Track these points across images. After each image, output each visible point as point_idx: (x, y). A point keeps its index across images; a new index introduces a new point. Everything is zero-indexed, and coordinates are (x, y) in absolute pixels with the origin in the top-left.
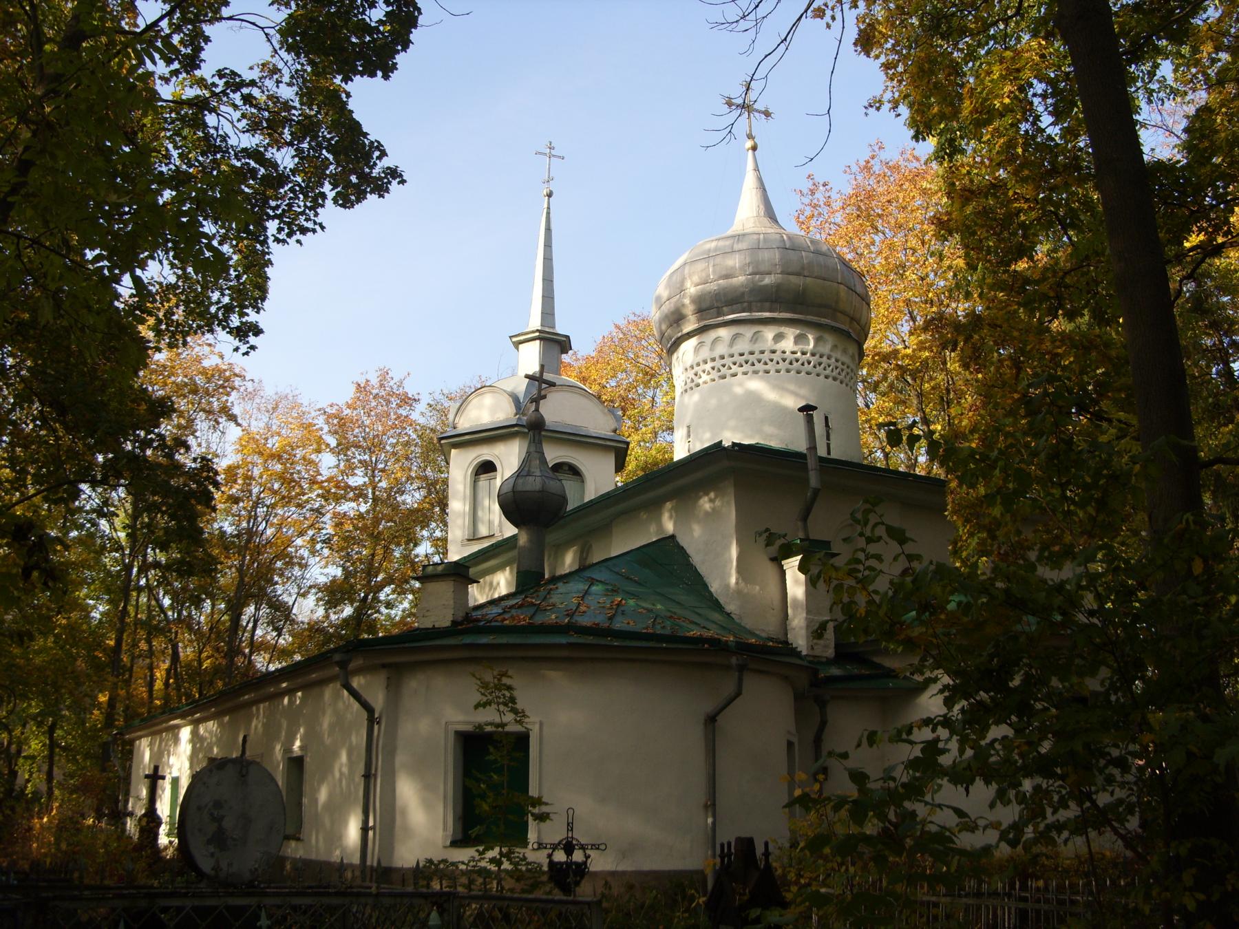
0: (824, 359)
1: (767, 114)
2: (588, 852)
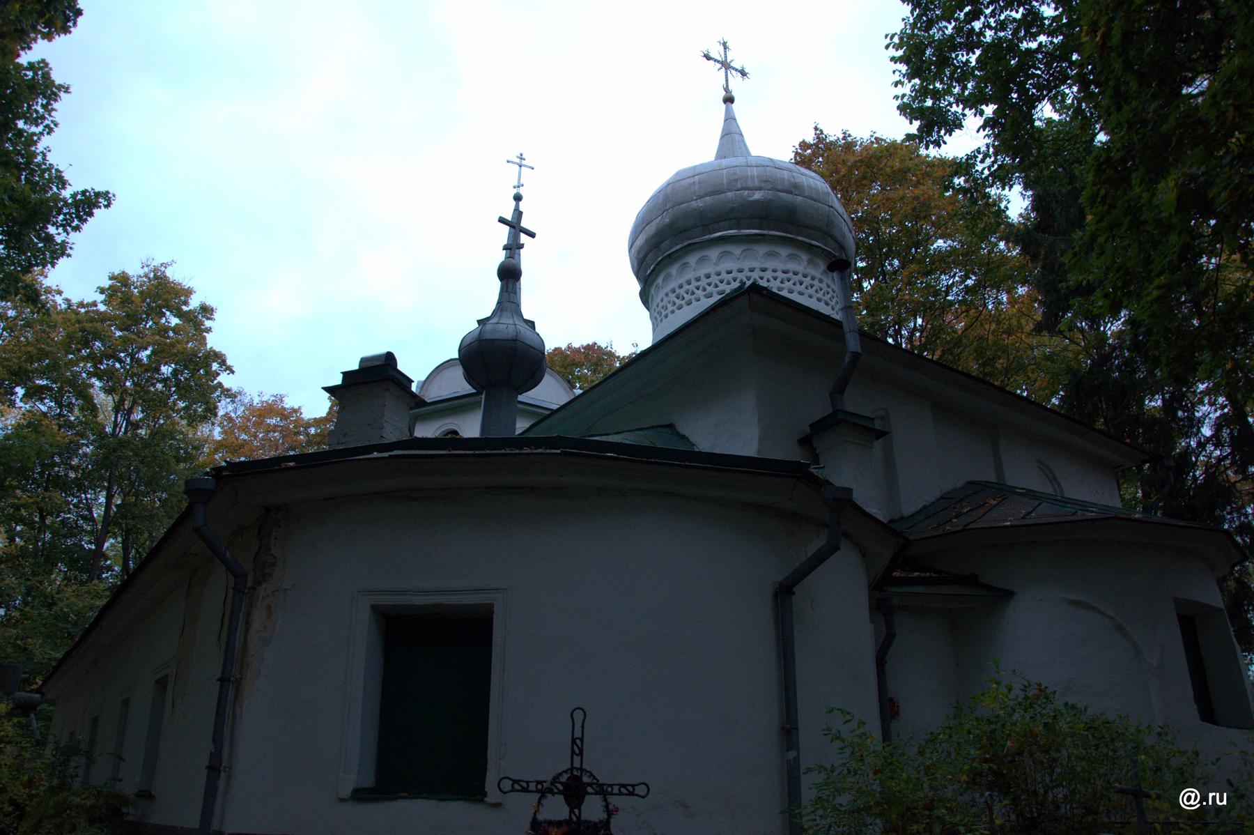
0: (816, 282)
1: (743, 73)
2: (614, 800)
